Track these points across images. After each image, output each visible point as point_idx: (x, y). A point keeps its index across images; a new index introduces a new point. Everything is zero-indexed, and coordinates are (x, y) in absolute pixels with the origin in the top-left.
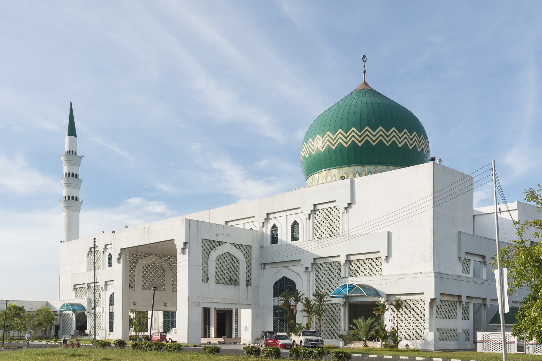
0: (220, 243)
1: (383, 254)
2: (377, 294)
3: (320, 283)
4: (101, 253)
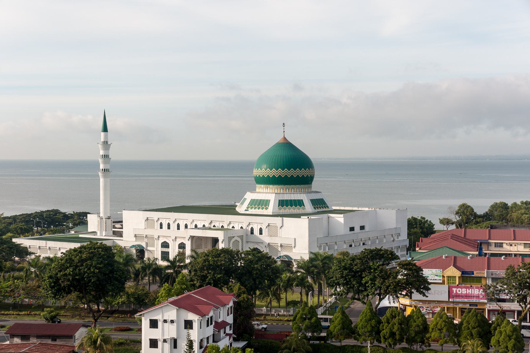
0: (233, 237)
1: (293, 245)
2: (291, 259)
3: (271, 252)
4: (156, 221)
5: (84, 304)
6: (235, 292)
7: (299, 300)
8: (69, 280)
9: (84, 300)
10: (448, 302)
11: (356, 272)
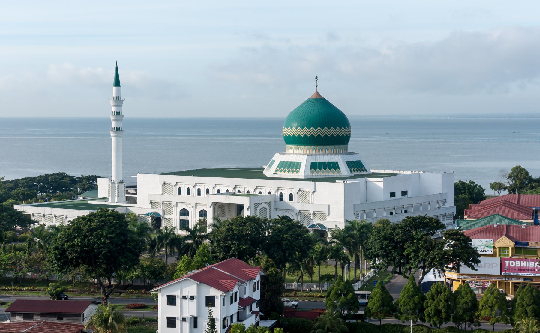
0: (260, 204)
1: (327, 213)
2: (325, 228)
4: (174, 186)
5: (94, 278)
6: (262, 265)
7: (334, 274)
8: (76, 252)
9: (94, 274)
10: (500, 276)
11: (397, 243)
